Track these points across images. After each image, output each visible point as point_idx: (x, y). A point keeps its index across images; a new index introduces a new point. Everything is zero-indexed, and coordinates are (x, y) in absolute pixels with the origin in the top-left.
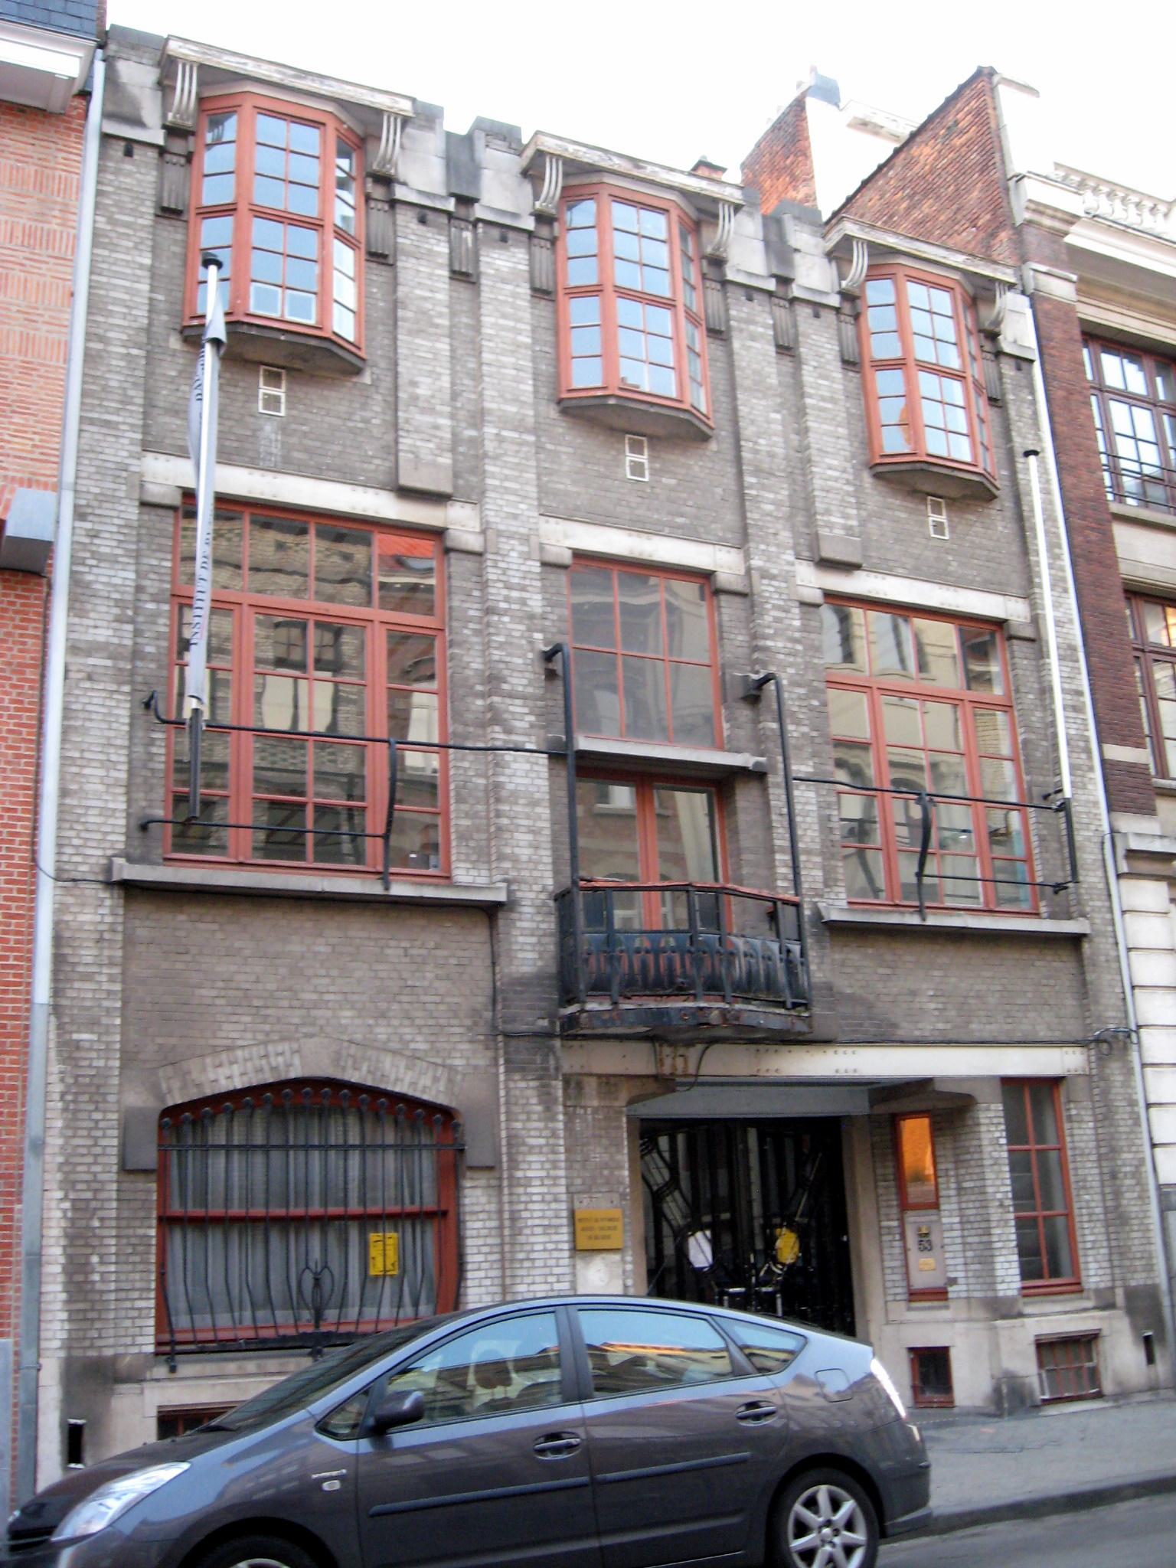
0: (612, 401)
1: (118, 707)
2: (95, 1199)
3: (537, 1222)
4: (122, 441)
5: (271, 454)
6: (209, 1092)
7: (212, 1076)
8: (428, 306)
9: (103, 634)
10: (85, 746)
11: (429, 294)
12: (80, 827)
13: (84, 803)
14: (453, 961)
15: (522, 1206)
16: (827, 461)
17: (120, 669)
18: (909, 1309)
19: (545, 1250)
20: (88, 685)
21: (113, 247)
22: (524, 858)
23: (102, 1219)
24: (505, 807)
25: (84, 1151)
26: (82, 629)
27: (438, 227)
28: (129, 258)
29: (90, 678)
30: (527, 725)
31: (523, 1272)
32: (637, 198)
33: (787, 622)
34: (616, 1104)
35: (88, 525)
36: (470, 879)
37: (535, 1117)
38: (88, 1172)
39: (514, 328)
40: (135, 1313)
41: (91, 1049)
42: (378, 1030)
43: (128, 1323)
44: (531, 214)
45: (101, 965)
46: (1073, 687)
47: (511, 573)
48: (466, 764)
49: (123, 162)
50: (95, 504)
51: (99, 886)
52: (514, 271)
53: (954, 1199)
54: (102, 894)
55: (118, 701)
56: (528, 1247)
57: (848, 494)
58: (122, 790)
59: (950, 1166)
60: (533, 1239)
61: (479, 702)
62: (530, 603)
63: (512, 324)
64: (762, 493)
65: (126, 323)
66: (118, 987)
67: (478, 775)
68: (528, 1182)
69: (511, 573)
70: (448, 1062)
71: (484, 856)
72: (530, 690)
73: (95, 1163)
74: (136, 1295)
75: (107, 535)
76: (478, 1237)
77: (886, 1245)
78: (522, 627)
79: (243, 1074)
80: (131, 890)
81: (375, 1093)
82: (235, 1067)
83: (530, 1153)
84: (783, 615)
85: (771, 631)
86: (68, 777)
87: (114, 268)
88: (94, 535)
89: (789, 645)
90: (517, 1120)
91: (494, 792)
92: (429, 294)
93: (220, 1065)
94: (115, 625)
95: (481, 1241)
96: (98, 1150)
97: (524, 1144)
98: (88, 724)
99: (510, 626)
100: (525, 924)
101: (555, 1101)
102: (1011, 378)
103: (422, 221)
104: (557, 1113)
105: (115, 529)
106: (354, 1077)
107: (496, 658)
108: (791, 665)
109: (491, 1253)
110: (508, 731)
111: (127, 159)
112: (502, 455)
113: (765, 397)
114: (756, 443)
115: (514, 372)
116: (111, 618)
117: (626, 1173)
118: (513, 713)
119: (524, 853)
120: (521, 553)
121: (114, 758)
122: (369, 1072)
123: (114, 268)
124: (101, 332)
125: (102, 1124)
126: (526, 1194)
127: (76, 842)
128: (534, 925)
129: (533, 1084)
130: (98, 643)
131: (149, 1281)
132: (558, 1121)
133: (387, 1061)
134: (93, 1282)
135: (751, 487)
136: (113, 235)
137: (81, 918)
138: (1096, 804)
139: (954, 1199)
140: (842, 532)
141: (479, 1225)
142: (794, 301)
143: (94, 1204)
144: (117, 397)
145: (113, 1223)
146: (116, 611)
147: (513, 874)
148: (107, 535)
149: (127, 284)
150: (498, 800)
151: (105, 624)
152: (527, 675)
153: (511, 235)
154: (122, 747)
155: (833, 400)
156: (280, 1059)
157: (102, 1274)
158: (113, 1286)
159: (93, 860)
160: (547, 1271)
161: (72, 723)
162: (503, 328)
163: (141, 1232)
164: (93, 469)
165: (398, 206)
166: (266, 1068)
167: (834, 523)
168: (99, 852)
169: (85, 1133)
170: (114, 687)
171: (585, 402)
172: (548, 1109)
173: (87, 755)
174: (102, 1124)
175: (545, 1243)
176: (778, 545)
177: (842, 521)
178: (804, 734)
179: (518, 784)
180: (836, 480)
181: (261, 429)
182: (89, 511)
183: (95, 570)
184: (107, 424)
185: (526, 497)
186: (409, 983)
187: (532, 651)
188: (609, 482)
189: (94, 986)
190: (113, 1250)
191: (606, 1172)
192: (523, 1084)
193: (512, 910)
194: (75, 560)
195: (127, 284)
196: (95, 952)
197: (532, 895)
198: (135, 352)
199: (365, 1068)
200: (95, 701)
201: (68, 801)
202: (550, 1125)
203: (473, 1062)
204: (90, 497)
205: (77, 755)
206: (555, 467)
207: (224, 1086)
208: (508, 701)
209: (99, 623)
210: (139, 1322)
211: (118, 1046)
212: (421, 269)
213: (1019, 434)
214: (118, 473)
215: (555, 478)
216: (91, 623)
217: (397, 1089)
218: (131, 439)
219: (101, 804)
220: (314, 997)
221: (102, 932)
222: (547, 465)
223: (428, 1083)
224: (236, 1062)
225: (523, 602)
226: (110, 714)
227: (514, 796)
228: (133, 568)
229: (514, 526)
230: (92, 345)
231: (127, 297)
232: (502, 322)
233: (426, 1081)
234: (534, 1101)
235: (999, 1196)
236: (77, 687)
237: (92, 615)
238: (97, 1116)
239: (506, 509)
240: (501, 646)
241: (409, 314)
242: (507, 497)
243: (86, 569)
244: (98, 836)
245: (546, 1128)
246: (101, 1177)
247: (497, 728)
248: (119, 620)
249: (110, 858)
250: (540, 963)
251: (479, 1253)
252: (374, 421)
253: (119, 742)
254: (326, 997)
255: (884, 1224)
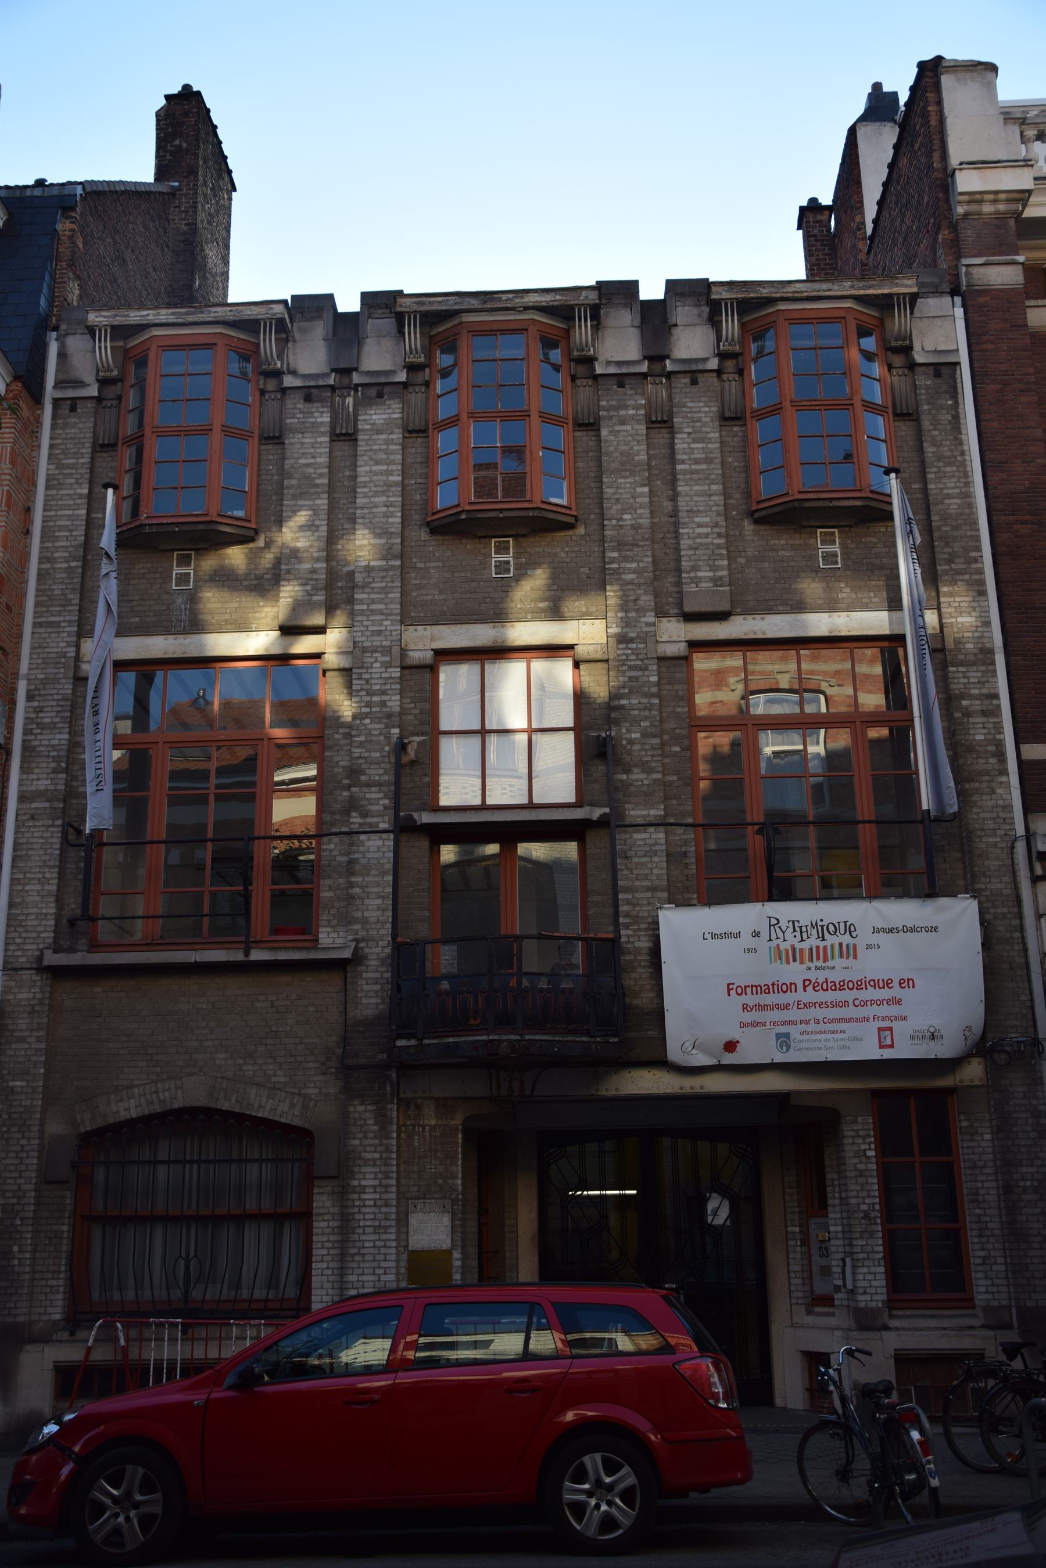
0: (463, 517)
1: (52, 837)
2: (18, 1204)
3: (368, 1223)
4: (62, 635)
5: (181, 621)
6: (111, 1121)
7: (114, 1109)
8: (311, 470)
9: (43, 784)
10: (27, 869)
11: (312, 461)
12: (21, 930)
13: (25, 911)
14: (312, 1009)
15: (356, 1210)
16: (696, 520)
17: (55, 809)
18: (809, 1313)
19: (374, 1247)
20: (31, 824)
21: (60, 486)
22: (373, 920)
23: (22, 1219)
24: (358, 879)
25: (12, 1168)
26: (29, 783)
27: (322, 400)
28: (72, 492)
29: (33, 818)
30: (382, 808)
31: (355, 1265)
32: (495, 327)
33: (645, 679)
34: (453, 1123)
35: (36, 704)
36: (332, 940)
37: (371, 1135)
38: (15, 1184)
39: (387, 470)
40: (48, 1290)
41: (22, 1093)
42: (246, 1068)
43: (42, 1297)
44: (404, 367)
45: (31, 1030)
46: (985, 691)
47: (373, 681)
48: (332, 846)
49: (69, 417)
50: (41, 686)
51: (33, 972)
52: (389, 422)
53: (838, 1209)
54: (34, 978)
55: (53, 832)
56: (360, 1244)
57: (719, 546)
58: (53, 899)
59: (835, 1176)
60: (363, 1238)
61: (345, 794)
62: (389, 704)
63: (385, 467)
64: (623, 565)
65: (68, 544)
66: (43, 1046)
67: (341, 854)
68: (363, 1189)
69: (373, 681)
70: (304, 1091)
71: (346, 920)
72: (386, 778)
73: (20, 1177)
74: (50, 1275)
75: (49, 709)
76: (323, 1234)
77: (791, 1249)
78: (381, 726)
79: (137, 1107)
80: (57, 973)
81: (242, 1118)
82: (132, 1101)
83: (365, 1165)
84: (640, 673)
85: (627, 691)
86: (15, 894)
87: (60, 503)
88: (39, 710)
89: (645, 701)
90: (354, 1138)
91: (350, 867)
92: (312, 461)
93: (121, 1100)
94: (51, 776)
95: (325, 1238)
96: (23, 1167)
97: (360, 1158)
98: (30, 853)
99: (370, 727)
100: (371, 975)
101: (391, 1122)
102: (928, 387)
103: (308, 399)
104: (392, 1132)
105: (55, 703)
106: (225, 1106)
107: (356, 755)
108: (646, 718)
109: (333, 1248)
110: (364, 815)
111: (73, 414)
112: (370, 583)
113: (632, 474)
114: (622, 519)
115: (385, 509)
116: (50, 771)
117: (460, 1182)
118: (369, 799)
119: (373, 915)
120: (382, 663)
121: (48, 875)
122: (237, 1101)
123: (60, 503)
124: (49, 554)
125: (27, 1148)
126: (360, 1199)
127: (18, 940)
128: (378, 975)
129: (370, 1108)
130: (40, 791)
131: (60, 1265)
132: (392, 1138)
133: (253, 1091)
134: (14, 1266)
135: (613, 560)
136: (61, 477)
137: (20, 996)
138: (1008, 807)
139: (838, 1209)
140: (710, 584)
141: (323, 1224)
142: (669, 375)
143: (17, 1207)
144: (58, 602)
145: (31, 1222)
146: (53, 765)
147: (362, 934)
148: (49, 709)
149: (70, 512)
150: (352, 874)
151: (45, 776)
152: (383, 765)
153: (387, 389)
154: (54, 867)
155: (708, 461)
156: (167, 1093)
157: (20, 1259)
158: (27, 1269)
159: (30, 953)
160: (376, 1264)
161: (19, 853)
162: (376, 473)
163: (55, 1228)
164: (40, 661)
165: (288, 392)
166: (156, 1101)
167: (700, 578)
168: (35, 947)
169: (14, 1155)
170: (51, 822)
171: (445, 521)
172: (383, 1128)
173: (28, 876)
174: (27, 1148)
175: (374, 1241)
176: (637, 611)
177: (711, 574)
178: (655, 781)
179: (369, 859)
180: (707, 536)
181: (174, 602)
182: (37, 692)
183: (39, 737)
184: (51, 624)
185: (390, 615)
186: (273, 1029)
187: (389, 744)
188: (474, 585)
189: (27, 1046)
190: (29, 1242)
191: (440, 1181)
192: (362, 1108)
193: (360, 964)
194: (26, 732)
195: (70, 512)
196: (28, 1021)
197: (379, 950)
198: (73, 564)
199: (234, 1099)
200: (36, 835)
201: (14, 911)
202: (385, 1141)
203: (324, 1091)
204: (37, 682)
205: (21, 876)
206: (424, 582)
207: (124, 1115)
208: (365, 790)
209: (41, 776)
210: (50, 1297)
211: (41, 1090)
212: (306, 440)
213: (934, 444)
214: (58, 660)
215: (423, 592)
216: (35, 777)
217: (260, 1115)
218: (68, 632)
219: (36, 910)
220: (196, 1044)
221: (33, 1006)
222: (418, 582)
223: (286, 1109)
224: (133, 1097)
225: (383, 704)
226: (46, 843)
227: (367, 869)
228: (67, 730)
229: (378, 641)
230: (43, 566)
231: (69, 523)
232: (375, 468)
233: (284, 1107)
234: (371, 1122)
235: (864, 1207)
236: (23, 826)
237: (36, 771)
238: (23, 1142)
239: (371, 628)
240: (361, 745)
241: (294, 482)
242: (372, 618)
243: (33, 737)
244: (34, 935)
245: (381, 1144)
246: (23, 1187)
247: (354, 814)
248: (55, 771)
249: (41, 951)
250: (381, 1007)
251: (323, 1248)
252: (266, 576)
253: (52, 863)
254: (205, 1044)
255: (790, 1229)
